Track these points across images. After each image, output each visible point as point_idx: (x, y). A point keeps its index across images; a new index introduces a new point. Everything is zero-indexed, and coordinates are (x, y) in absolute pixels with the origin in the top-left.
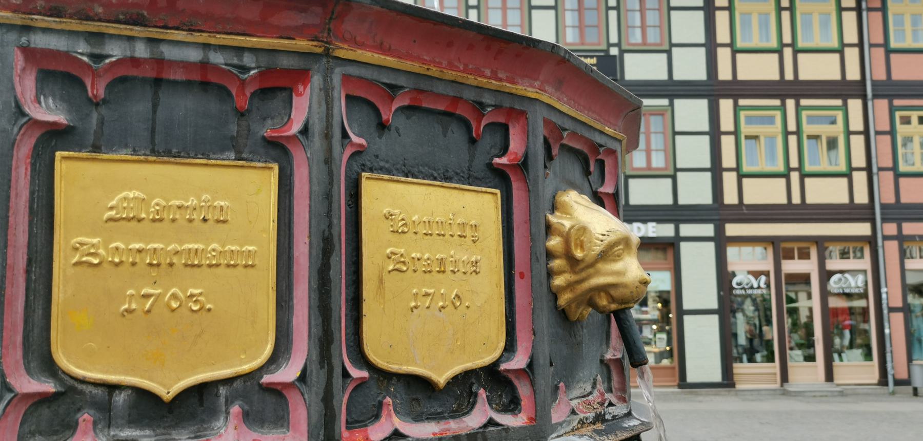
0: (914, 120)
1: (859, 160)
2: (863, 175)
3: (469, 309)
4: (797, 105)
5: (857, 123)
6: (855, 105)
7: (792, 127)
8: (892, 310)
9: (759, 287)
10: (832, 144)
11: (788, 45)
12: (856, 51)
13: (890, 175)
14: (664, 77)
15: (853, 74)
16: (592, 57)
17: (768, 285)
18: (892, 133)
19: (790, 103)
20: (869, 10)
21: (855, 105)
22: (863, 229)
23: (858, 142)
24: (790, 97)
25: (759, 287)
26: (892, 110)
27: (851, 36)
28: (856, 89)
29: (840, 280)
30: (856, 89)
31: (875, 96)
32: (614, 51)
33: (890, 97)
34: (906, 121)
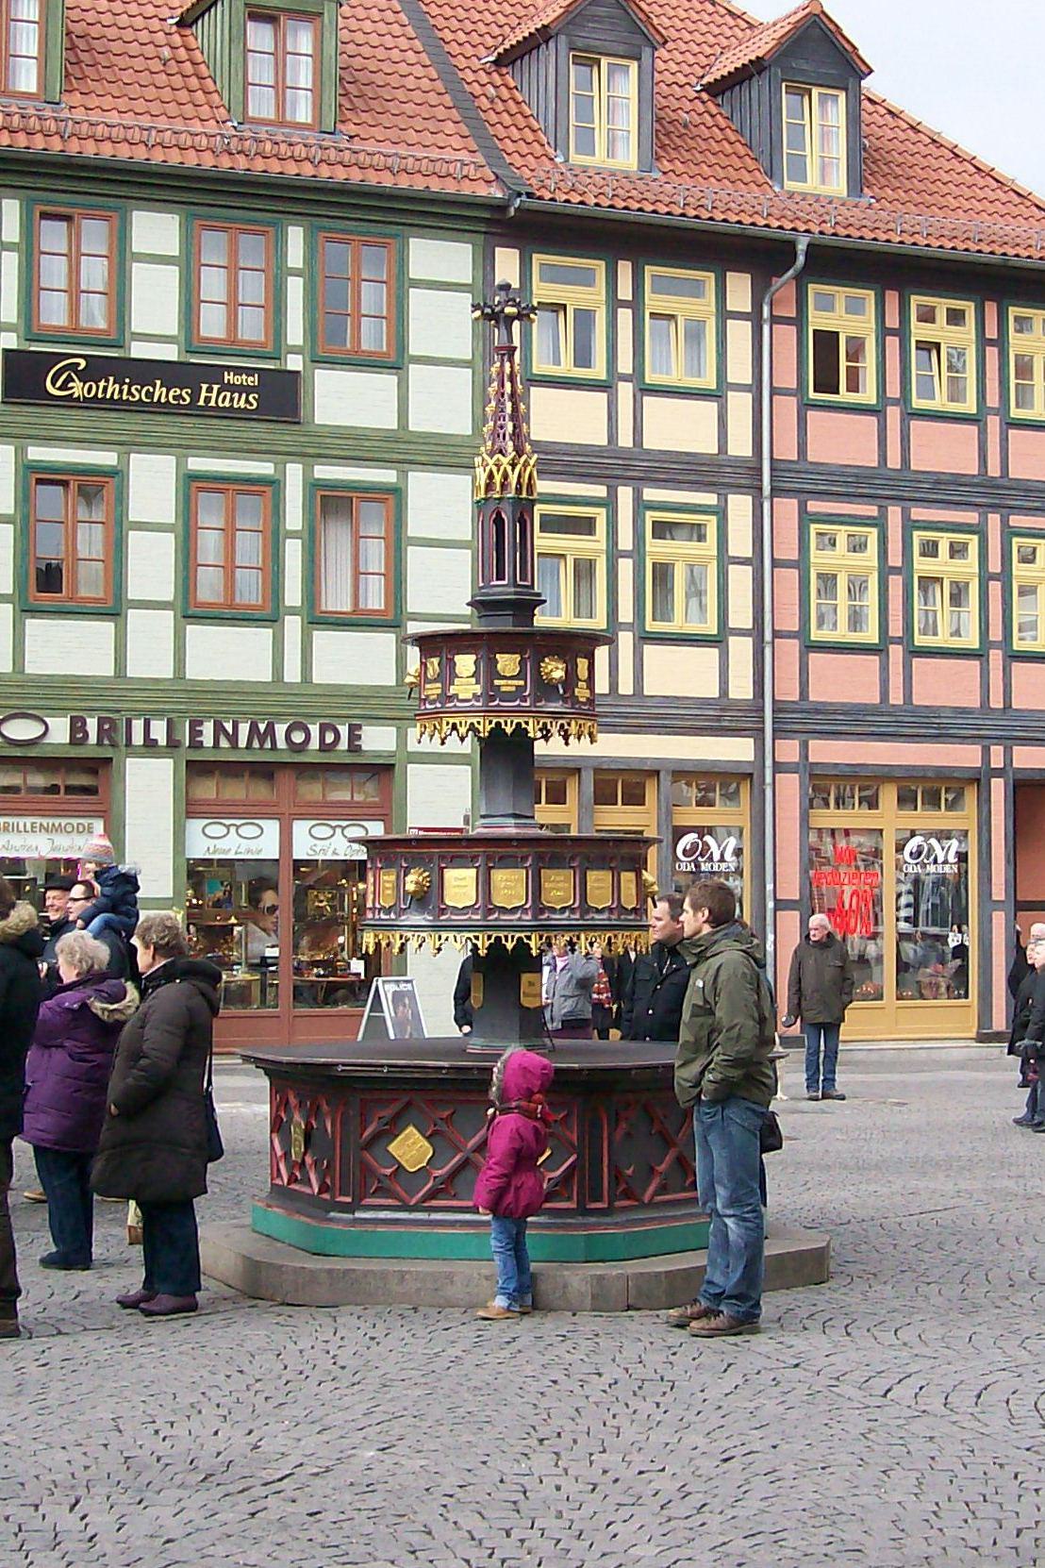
0: (842, 541)
1: (741, 615)
2: (747, 643)
3: (895, 881)
4: (1005, 523)
5: (741, 544)
6: (740, 506)
7: (895, 559)
8: (780, 905)
9: (945, 862)
10: (957, 597)
11: (625, 378)
12: (747, 398)
13: (794, 645)
14: (602, 440)
15: (740, 446)
16: (250, 372)
17: (962, 857)
18: (802, 564)
19: (625, 494)
20: (775, 320)
21: (740, 506)
22: (738, 750)
23: (741, 579)
24: (627, 480)
25: (945, 862)
26: (805, 518)
27: (740, 370)
28: (743, 476)
29: (695, 846)
30: (743, 476)
31: (776, 491)
32: (294, 363)
33: (803, 495)
34: (930, 550)
